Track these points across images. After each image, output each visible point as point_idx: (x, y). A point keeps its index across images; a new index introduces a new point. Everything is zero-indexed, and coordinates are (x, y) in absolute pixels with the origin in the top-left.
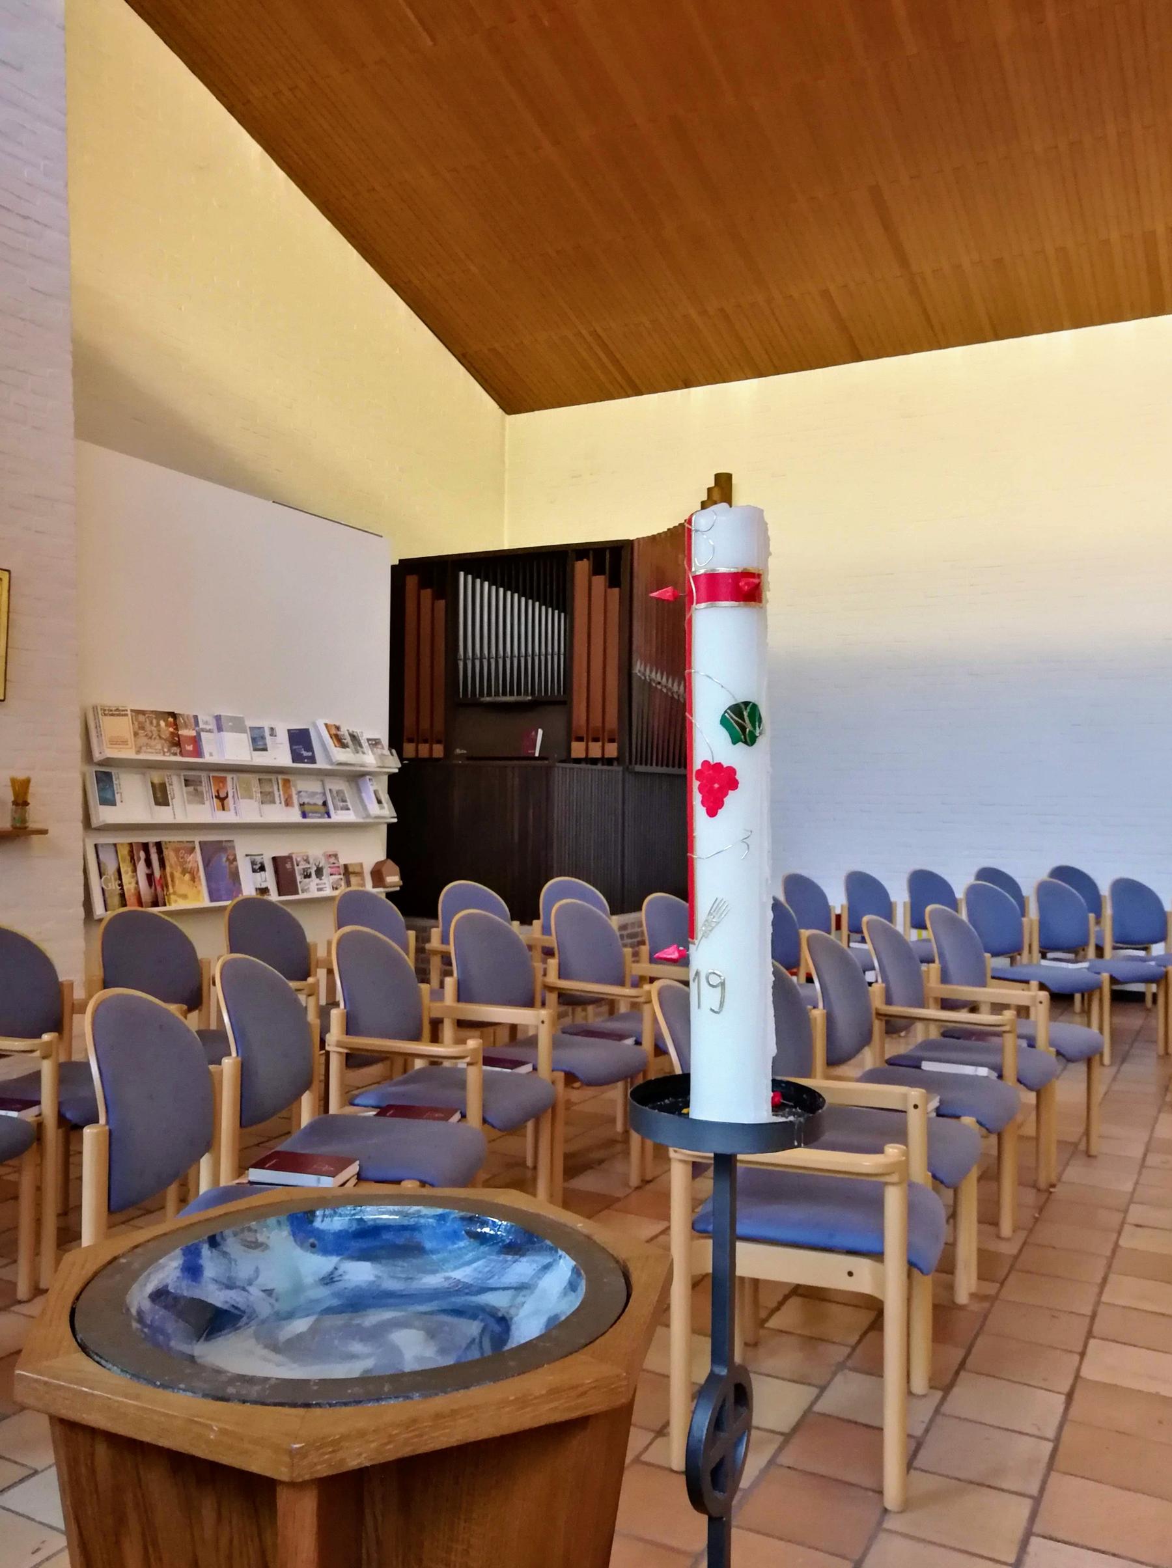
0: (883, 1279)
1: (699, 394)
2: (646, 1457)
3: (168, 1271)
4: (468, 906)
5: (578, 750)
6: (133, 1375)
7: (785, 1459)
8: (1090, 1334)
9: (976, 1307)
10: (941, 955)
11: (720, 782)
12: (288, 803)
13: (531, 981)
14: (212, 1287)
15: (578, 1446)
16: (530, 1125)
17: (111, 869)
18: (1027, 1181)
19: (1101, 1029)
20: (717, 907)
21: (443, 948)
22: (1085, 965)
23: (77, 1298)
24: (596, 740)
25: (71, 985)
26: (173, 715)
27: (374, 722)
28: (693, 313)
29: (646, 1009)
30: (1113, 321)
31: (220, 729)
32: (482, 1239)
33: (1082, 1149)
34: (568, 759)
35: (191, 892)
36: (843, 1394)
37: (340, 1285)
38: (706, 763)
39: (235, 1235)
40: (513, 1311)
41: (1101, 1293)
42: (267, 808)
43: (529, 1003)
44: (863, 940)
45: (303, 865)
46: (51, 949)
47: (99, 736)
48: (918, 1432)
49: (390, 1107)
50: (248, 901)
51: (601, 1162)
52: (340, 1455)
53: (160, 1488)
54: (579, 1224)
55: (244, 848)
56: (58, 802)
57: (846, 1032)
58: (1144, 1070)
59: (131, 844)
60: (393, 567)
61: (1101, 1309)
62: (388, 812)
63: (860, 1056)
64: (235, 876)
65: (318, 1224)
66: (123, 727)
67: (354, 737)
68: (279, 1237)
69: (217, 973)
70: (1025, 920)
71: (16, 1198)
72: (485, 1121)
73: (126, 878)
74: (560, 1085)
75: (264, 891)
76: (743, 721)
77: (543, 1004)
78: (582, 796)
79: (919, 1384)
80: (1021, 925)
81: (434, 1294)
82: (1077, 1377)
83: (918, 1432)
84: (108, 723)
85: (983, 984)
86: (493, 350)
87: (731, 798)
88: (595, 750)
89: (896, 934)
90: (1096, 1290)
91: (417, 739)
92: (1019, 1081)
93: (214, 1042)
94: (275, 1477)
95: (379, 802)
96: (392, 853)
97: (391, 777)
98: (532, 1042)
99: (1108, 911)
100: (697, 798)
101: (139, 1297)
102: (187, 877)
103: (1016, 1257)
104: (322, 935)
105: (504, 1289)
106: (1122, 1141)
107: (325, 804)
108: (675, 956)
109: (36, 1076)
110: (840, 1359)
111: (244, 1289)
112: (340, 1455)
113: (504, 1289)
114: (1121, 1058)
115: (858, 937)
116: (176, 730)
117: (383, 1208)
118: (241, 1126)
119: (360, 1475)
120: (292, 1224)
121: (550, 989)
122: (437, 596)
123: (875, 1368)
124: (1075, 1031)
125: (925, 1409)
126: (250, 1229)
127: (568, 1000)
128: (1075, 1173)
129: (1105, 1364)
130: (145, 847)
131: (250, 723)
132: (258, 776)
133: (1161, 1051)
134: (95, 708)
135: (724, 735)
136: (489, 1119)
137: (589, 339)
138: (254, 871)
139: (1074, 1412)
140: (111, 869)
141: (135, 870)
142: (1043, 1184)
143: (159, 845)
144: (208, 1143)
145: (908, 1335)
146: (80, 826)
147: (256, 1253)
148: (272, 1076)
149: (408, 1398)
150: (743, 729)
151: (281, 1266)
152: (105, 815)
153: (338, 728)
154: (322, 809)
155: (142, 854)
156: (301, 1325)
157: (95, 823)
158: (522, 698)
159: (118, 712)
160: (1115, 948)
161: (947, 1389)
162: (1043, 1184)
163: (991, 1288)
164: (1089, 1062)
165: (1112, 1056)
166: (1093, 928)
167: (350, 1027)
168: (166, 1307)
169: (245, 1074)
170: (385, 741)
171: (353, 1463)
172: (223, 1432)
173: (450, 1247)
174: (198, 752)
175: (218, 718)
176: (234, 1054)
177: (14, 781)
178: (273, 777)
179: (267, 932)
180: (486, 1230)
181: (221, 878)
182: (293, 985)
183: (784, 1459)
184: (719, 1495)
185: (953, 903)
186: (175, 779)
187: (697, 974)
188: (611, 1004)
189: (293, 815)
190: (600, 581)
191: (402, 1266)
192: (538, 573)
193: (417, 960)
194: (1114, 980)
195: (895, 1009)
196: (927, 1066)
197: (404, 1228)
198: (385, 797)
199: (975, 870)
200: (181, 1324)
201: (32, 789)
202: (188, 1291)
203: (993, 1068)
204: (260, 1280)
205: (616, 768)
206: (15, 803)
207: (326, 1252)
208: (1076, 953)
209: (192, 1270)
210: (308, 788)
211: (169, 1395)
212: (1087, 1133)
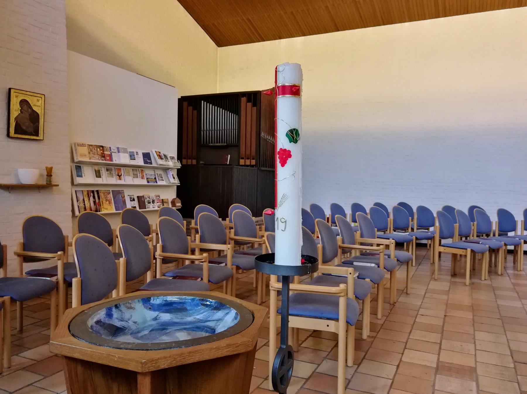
0: (339, 327)
1: (284, 41)
2: (260, 387)
3: (101, 315)
4: (204, 212)
5: (242, 162)
6: (89, 343)
7: (306, 386)
8: (405, 348)
9: (370, 340)
10: (361, 228)
11: (286, 155)
12: (142, 178)
13: (225, 235)
14: (116, 321)
15: (237, 364)
16: (225, 282)
17: (81, 199)
18: (386, 301)
19: (412, 254)
20: (284, 196)
21: (196, 227)
22: (408, 233)
23: (71, 322)
24: (248, 159)
25: (68, 237)
26: (102, 147)
27: (172, 150)
28: (282, 13)
29: (264, 246)
30: (419, 20)
31: (119, 152)
32: (207, 306)
33: (404, 292)
34: (239, 165)
35: (109, 207)
36: (325, 366)
37: (159, 321)
38: (281, 149)
39: (124, 304)
40: (216, 327)
41: (409, 336)
42: (135, 179)
43: (225, 243)
44: (336, 226)
45: (148, 199)
46: (61, 225)
47: (76, 153)
48: (349, 377)
49: (177, 276)
50: (129, 210)
51: (248, 296)
52: (158, 364)
53: (99, 379)
54: (239, 301)
55: (127, 193)
56: (62, 174)
57: (329, 254)
58: (425, 268)
59: (88, 191)
60: (179, 99)
61: (409, 340)
62: (177, 182)
63: (333, 261)
64: (124, 202)
65: (152, 301)
66: (84, 150)
67: (165, 156)
68: (139, 306)
69: (118, 233)
70: (389, 219)
71: (50, 309)
72: (209, 281)
73: (86, 202)
74: (234, 271)
75: (135, 207)
76: (294, 135)
77: (229, 244)
78: (243, 176)
79: (350, 363)
80: (387, 221)
81: (190, 323)
82: (401, 360)
83: (349, 377)
84: (79, 148)
85: (375, 238)
86: (214, 24)
87: (289, 161)
88: (248, 162)
89: (347, 222)
90: (408, 334)
91: (187, 158)
92: (385, 268)
93: (118, 256)
94: (137, 371)
95: (174, 178)
96: (178, 195)
97: (178, 170)
98: (226, 256)
99: (416, 217)
100: (278, 161)
101: (91, 322)
102: (108, 202)
103: (382, 325)
104: (154, 222)
105: (213, 321)
106: (418, 289)
107: (155, 178)
108: (270, 213)
109: (56, 267)
110: (325, 356)
111: (127, 321)
112: (158, 364)
113: (213, 321)
114: (419, 264)
115: (335, 225)
116: (103, 152)
117: (174, 297)
118: (127, 281)
119: (165, 371)
120: (143, 302)
121: (232, 239)
122: (194, 109)
123: (336, 359)
124: (403, 254)
125: (351, 371)
126: (129, 303)
127: (237, 243)
128: (402, 299)
129: (410, 356)
130: (93, 192)
131: (129, 150)
132: (132, 168)
133: (432, 262)
134: (75, 144)
135: (287, 140)
136: (210, 280)
137: (247, 21)
138: (131, 201)
139: (399, 371)
140: (81, 199)
141: (89, 200)
142: (392, 302)
143: (97, 191)
144: (115, 286)
145: (346, 348)
146: (70, 184)
147: (131, 310)
148: (136, 268)
149: (181, 347)
150: (293, 138)
151: (139, 315)
152: (79, 180)
153: (160, 153)
154: (154, 180)
155: (92, 194)
156: (146, 332)
157: (75, 183)
158: (223, 144)
159: (83, 145)
160: (417, 229)
161: (359, 365)
162: (392, 302)
163: (374, 334)
164: (408, 263)
165: (416, 263)
166: (411, 223)
167: (164, 250)
168: (100, 326)
169: (128, 264)
170: (176, 157)
171: (162, 367)
172: (119, 358)
173: (196, 309)
174: (111, 160)
175: (118, 148)
176: (124, 257)
177: (47, 168)
178: (137, 169)
179: (136, 220)
180: (208, 303)
181: (119, 202)
182: (146, 237)
183: (305, 386)
184: (283, 386)
185: (366, 213)
186: (103, 169)
187: (277, 218)
188: (253, 244)
189: (145, 182)
190: (249, 105)
191: (180, 315)
192: (229, 101)
193: (187, 229)
194: (417, 239)
195: (346, 245)
196: (355, 263)
197: (181, 303)
198: (176, 176)
199: (373, 203)
200: (106, 331)
201: (53, 171)
202: (108, 321)
203: (376, 264)
204: (132, 319)
205: (255, 168)
206: (47, 175)
207: (154, 310)
208: (405, 230)
209: (109, 315)
210: (149, 173)
211: (102, 347)
212: (407, 287)
